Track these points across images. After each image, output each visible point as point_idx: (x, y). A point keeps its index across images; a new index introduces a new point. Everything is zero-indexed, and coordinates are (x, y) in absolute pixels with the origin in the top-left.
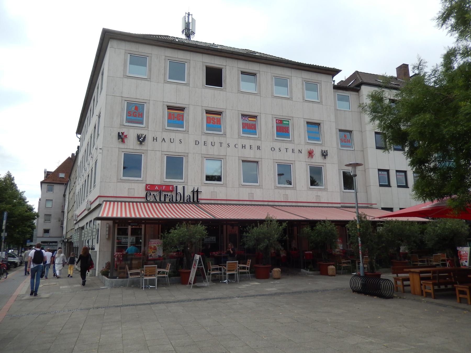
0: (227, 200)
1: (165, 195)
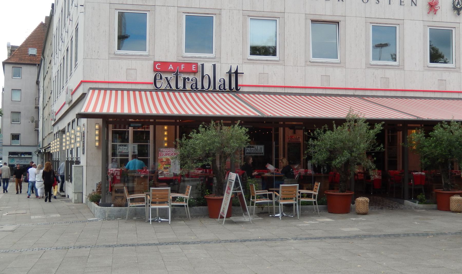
0: (285, 87)
1: (185, 79)
